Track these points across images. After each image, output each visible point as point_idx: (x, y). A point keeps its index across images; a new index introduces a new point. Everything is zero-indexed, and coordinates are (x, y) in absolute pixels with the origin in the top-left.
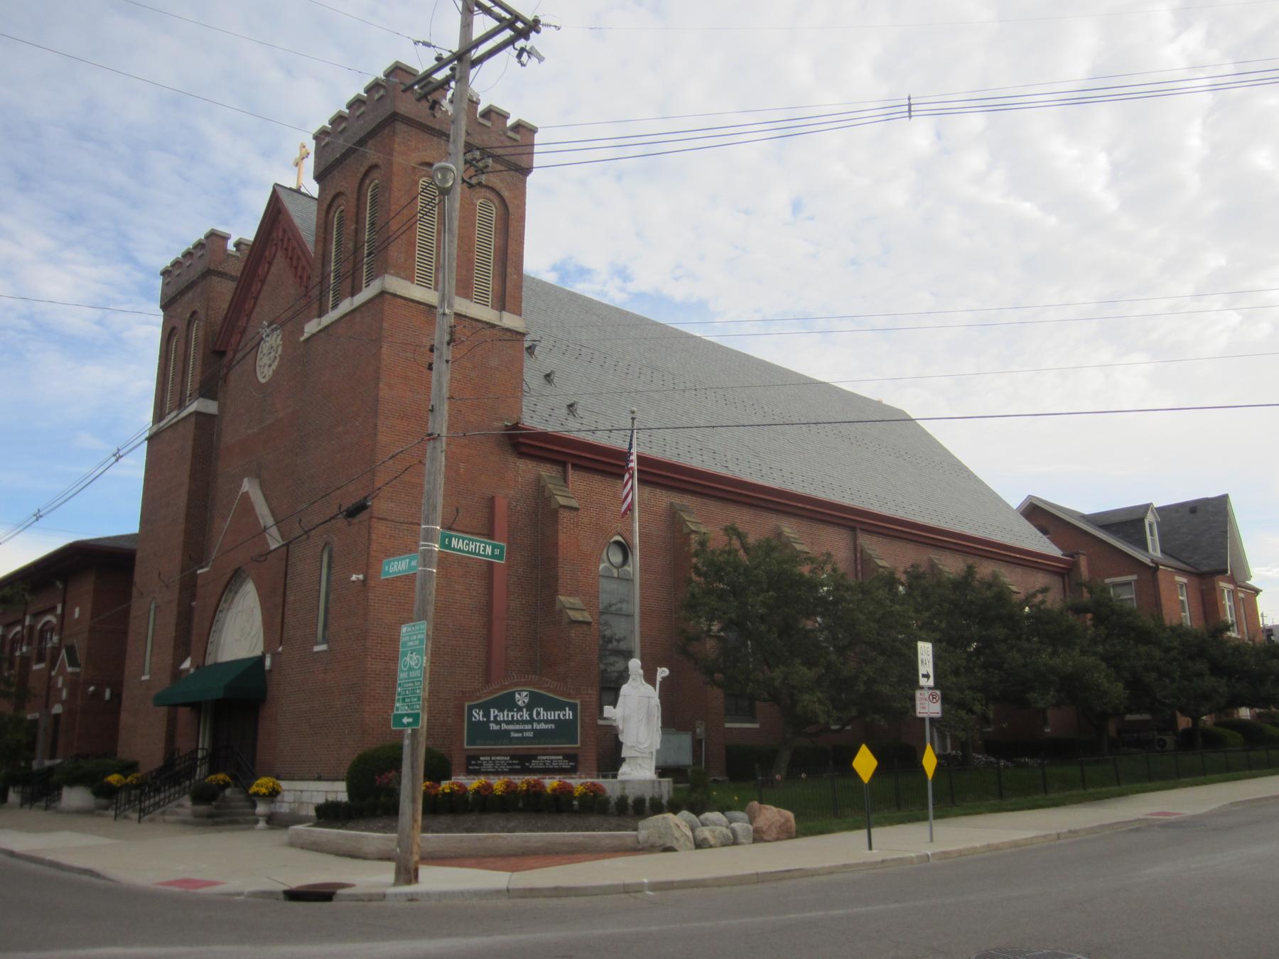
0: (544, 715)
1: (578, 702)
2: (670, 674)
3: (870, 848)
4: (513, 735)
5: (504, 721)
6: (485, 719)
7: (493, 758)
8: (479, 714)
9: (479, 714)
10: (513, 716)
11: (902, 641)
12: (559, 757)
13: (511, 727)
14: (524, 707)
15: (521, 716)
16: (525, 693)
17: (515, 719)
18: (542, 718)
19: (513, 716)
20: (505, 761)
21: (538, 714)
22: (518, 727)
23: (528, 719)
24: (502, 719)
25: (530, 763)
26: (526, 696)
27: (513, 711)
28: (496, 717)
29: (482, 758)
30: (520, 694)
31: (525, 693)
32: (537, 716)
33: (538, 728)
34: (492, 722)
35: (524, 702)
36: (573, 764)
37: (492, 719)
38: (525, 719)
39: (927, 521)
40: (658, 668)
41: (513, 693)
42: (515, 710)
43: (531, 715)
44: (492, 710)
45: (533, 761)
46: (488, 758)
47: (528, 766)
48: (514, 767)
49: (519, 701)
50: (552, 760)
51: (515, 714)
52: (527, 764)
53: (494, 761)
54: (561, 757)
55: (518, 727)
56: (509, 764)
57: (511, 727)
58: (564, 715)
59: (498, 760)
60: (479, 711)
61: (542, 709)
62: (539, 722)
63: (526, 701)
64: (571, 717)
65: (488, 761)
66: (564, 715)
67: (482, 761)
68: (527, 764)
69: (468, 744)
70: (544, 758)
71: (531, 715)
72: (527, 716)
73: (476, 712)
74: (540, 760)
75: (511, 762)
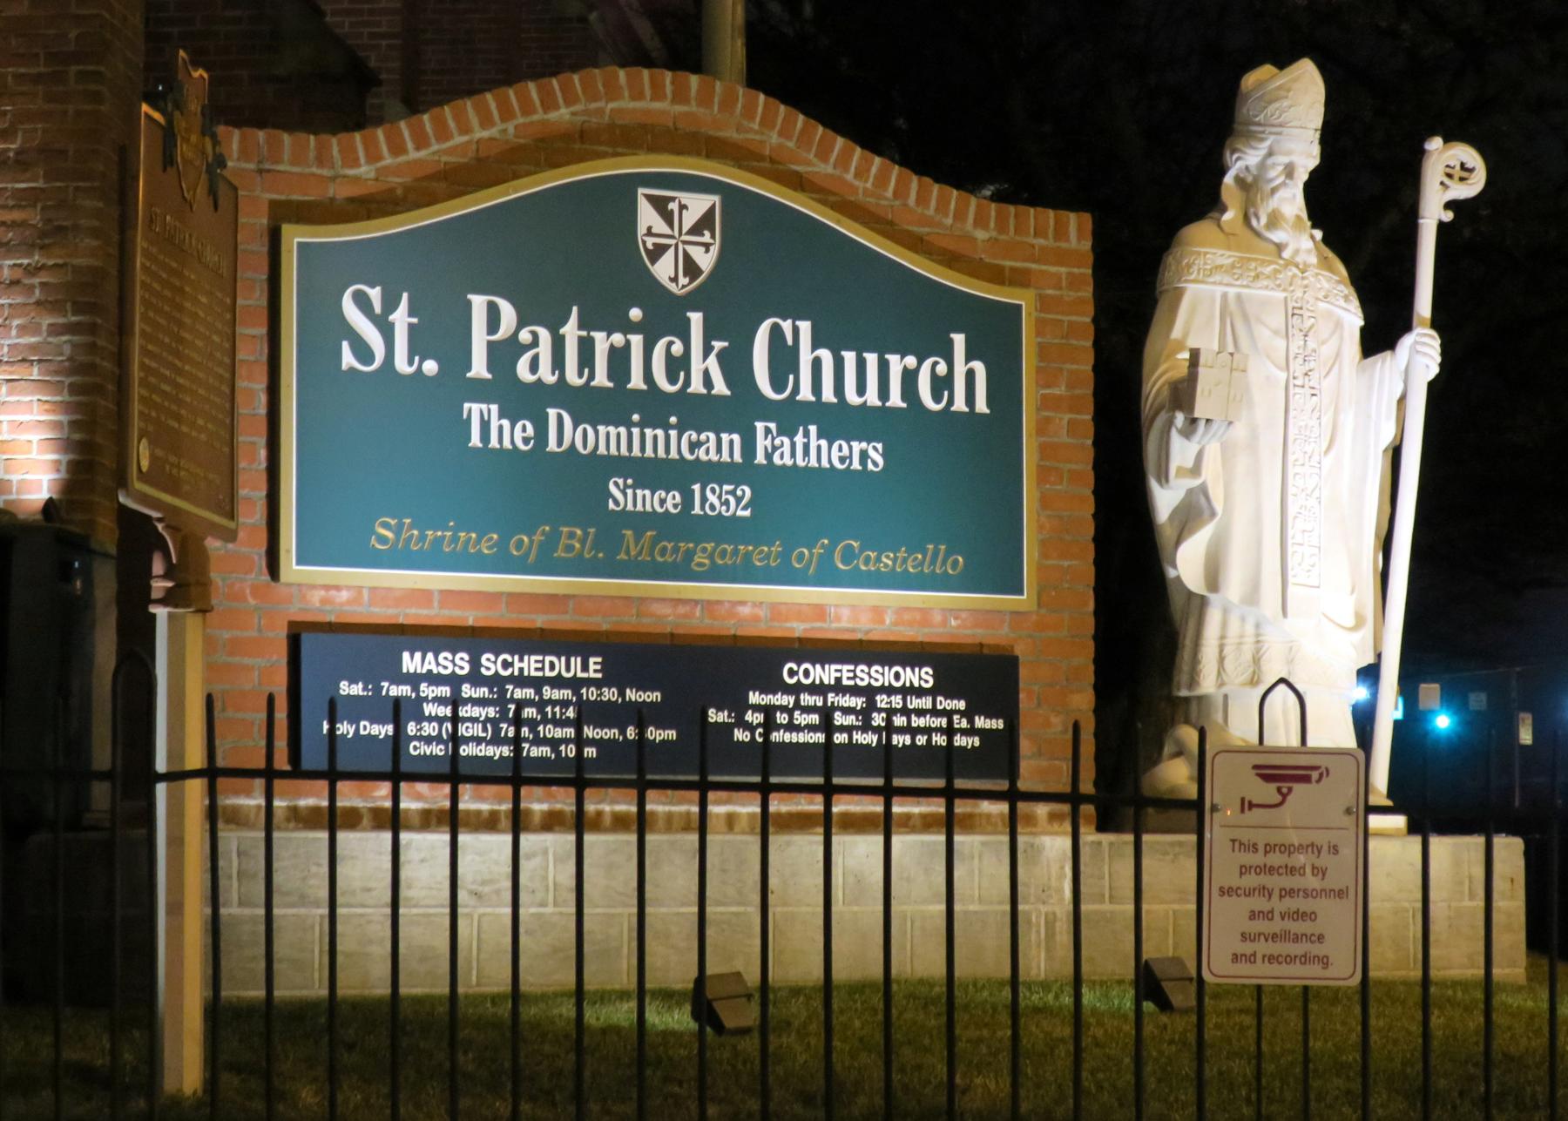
0: (817, 364)
1: (1023, 300)
2: (1455, 216)
3: (1221, 826)
4: (622, 496)
5: (561, 394)
6: (430, 367)
7: (491, 664)
8: (387, 331)
9: (387, 331)
10: (619, 359)
11: (349, 602)
12: (910, 676)
13: (609, 439)
14: (691, 301)
15: (678, 366)
16: (697, 205)
17: (637, 381)
18: (806, 394)
19: (619, 359)
20: (575, 684)
21: (784, 360)
22: (657, 442)
23: (720, 387)
24: (547, 375)
25: (739, 706)
26: (705, 223)
27: (628, 327)
28: (504, 353)
29: (411, 663)
30: (660, 205)
31: (697, 205)
32: (778, 383)
33: (783, 459)
34: (480, 391)
35: (691, 269)
36: (998, 724)
37: (479, 368)
38: (696, 386)
39: (391, 611)
40: (1435, 144)
41: (624, 189)
42: (635, 314)
43: (736, 365)
44: (478, 302)
45: (755, 698)
46: (460, 663)
47: (727, 729)
48: (88, 184)
49: (657, 252)
50: (869, 692)
51: (636, 340)
52: (716, 716)
53: (496, 681)
54: (923, 676)
55: (657, 442)
56: (590, 713)
57: (609, 439)
58: (942, 385)
59: (521, 681)
60: (390, 304)
61: (805, 327)
62: (790, 417)
63: (706, 260)
64: (981, 406)
65: (454, 681)
66: (942, 385)
67: (414, 680)
68: (716, 716)
69: (1022, 594)
70: (825, 674)
71: (736, 365)
72: (712, 363)
73: (362, 302)
74: (797, 689)
75: (610, 694)
